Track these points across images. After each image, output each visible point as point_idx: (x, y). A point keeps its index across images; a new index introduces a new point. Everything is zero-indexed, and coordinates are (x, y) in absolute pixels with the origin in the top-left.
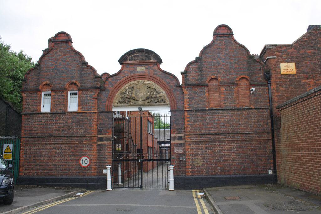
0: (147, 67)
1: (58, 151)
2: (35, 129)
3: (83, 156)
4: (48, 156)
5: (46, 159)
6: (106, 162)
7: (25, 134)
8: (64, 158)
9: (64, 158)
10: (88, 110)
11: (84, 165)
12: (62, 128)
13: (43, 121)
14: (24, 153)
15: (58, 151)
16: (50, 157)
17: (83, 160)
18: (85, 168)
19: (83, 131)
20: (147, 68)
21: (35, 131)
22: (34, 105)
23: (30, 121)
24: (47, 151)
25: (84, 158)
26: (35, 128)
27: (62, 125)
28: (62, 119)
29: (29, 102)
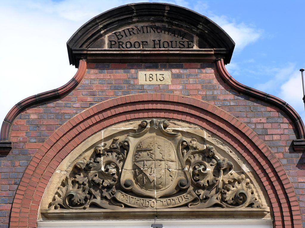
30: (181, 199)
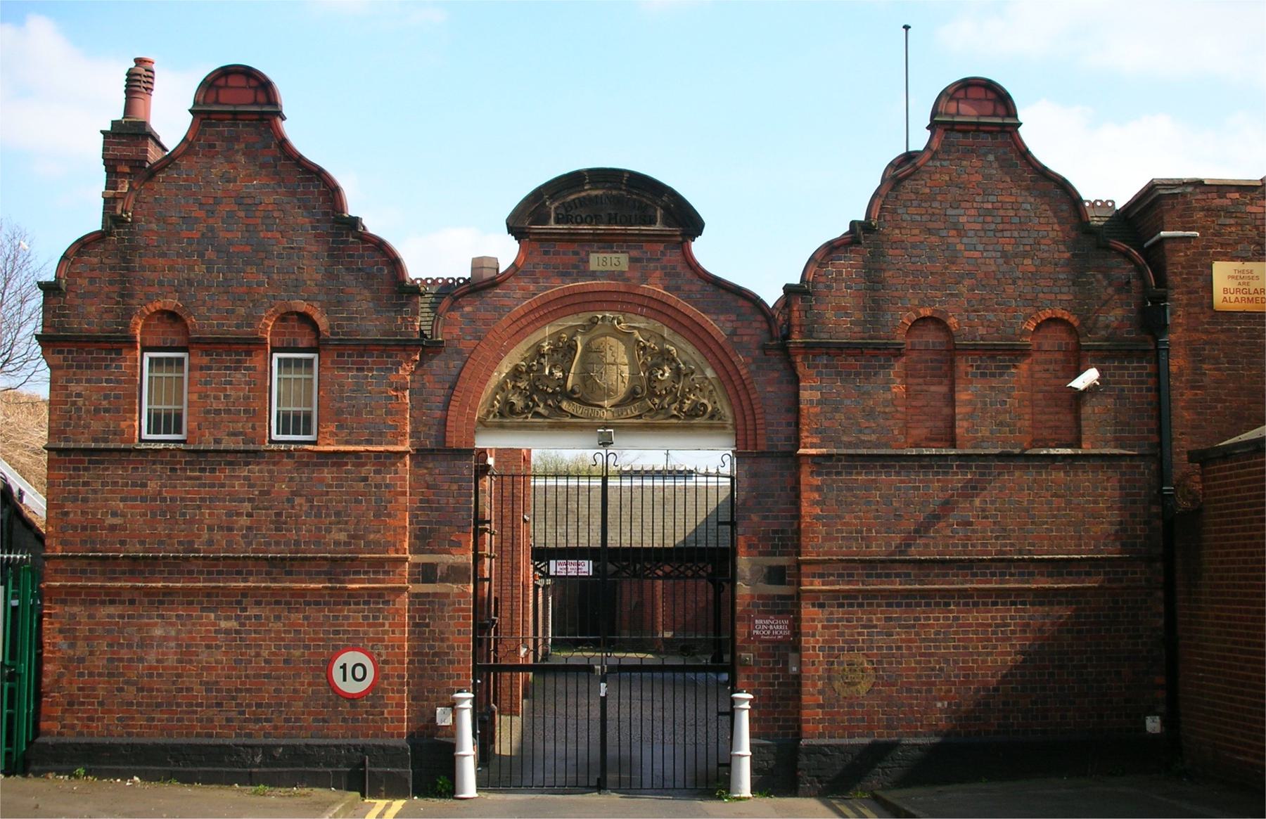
0: (635, 253)
1: (224, 624)
2: (110, 520)
3: (347, 649)
4: (179, 646)
5: (172, 660)
6: (450, 677)
7: (64, 543)
8: (258, 655)
9: (258, 655)
10: (369, 442)
11: (351, 687)
12: (244, 521)
13: (152, 486)
14: (61, 631)
15: (224, 624)
16: (186, 654)
17: (344, 667)
18: (352, 699)
19: (343, 537)
20: (632, 260)
21: (113, 528)
22: (106, 411)
23: (86, 484)
24: (173, 624)
25: (350, 658)
26: (114, 514)
27: (247, 506)
28: (245, 478)
29: (79, 395)
30: (633, 410)
